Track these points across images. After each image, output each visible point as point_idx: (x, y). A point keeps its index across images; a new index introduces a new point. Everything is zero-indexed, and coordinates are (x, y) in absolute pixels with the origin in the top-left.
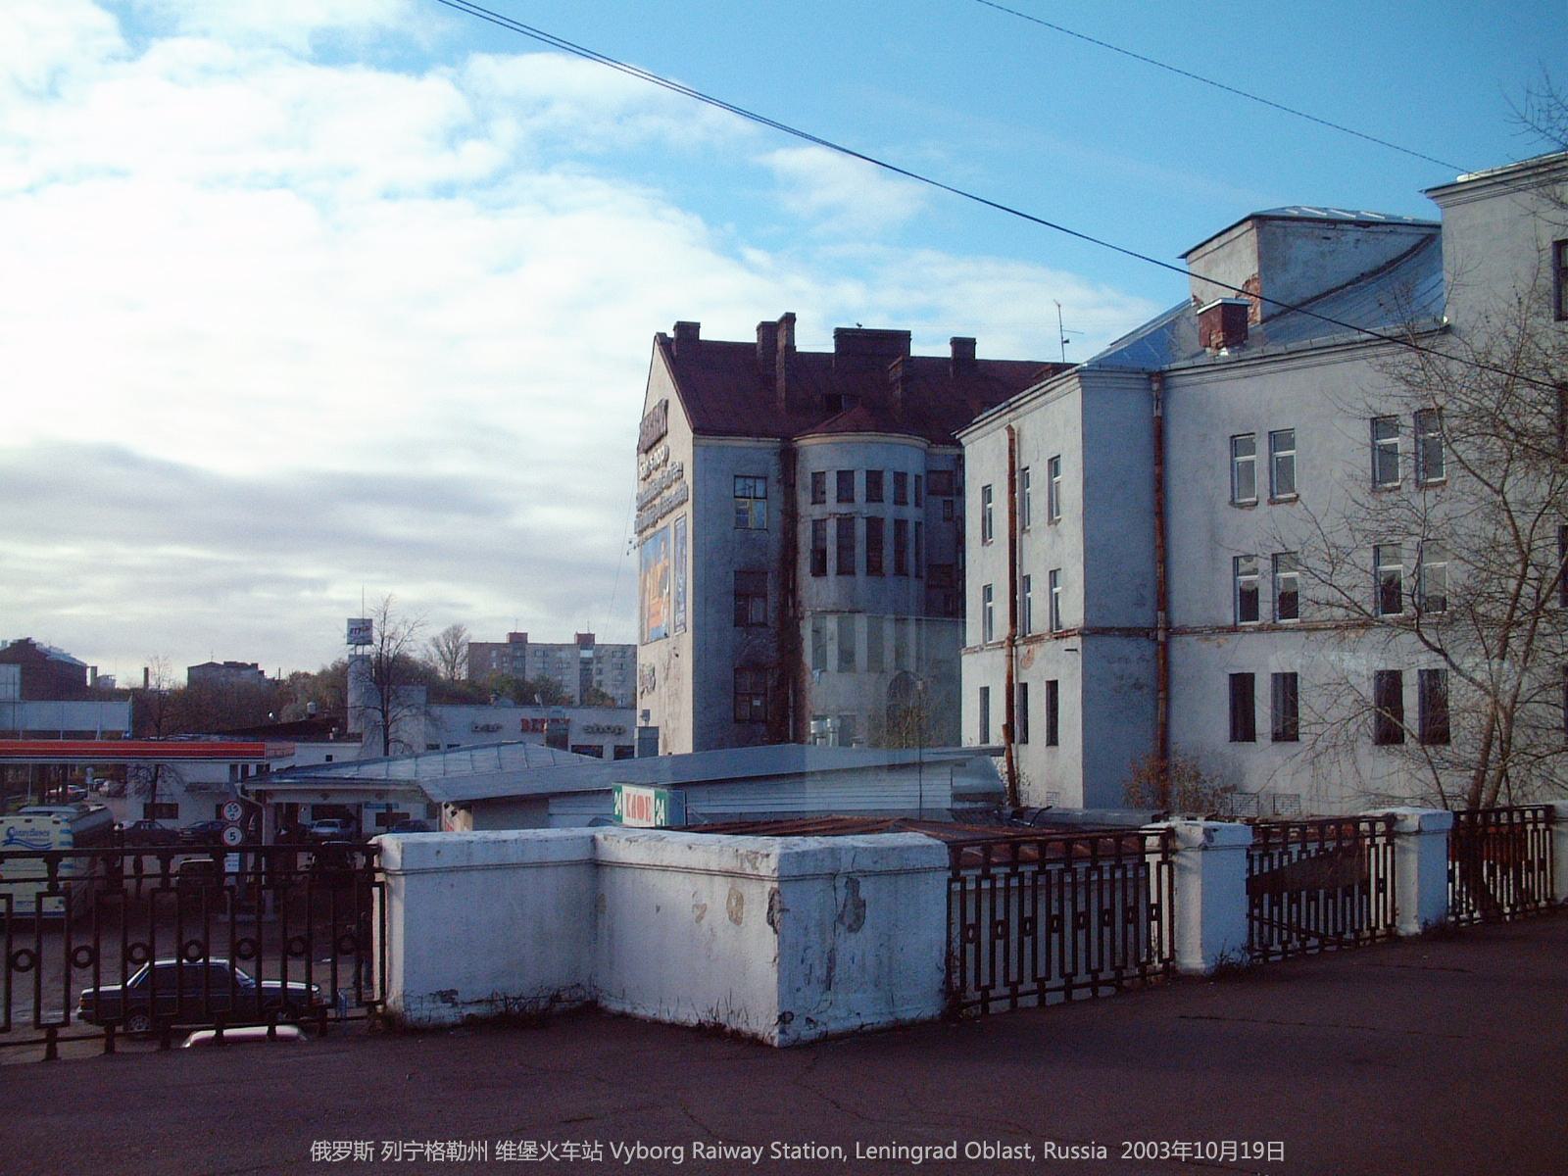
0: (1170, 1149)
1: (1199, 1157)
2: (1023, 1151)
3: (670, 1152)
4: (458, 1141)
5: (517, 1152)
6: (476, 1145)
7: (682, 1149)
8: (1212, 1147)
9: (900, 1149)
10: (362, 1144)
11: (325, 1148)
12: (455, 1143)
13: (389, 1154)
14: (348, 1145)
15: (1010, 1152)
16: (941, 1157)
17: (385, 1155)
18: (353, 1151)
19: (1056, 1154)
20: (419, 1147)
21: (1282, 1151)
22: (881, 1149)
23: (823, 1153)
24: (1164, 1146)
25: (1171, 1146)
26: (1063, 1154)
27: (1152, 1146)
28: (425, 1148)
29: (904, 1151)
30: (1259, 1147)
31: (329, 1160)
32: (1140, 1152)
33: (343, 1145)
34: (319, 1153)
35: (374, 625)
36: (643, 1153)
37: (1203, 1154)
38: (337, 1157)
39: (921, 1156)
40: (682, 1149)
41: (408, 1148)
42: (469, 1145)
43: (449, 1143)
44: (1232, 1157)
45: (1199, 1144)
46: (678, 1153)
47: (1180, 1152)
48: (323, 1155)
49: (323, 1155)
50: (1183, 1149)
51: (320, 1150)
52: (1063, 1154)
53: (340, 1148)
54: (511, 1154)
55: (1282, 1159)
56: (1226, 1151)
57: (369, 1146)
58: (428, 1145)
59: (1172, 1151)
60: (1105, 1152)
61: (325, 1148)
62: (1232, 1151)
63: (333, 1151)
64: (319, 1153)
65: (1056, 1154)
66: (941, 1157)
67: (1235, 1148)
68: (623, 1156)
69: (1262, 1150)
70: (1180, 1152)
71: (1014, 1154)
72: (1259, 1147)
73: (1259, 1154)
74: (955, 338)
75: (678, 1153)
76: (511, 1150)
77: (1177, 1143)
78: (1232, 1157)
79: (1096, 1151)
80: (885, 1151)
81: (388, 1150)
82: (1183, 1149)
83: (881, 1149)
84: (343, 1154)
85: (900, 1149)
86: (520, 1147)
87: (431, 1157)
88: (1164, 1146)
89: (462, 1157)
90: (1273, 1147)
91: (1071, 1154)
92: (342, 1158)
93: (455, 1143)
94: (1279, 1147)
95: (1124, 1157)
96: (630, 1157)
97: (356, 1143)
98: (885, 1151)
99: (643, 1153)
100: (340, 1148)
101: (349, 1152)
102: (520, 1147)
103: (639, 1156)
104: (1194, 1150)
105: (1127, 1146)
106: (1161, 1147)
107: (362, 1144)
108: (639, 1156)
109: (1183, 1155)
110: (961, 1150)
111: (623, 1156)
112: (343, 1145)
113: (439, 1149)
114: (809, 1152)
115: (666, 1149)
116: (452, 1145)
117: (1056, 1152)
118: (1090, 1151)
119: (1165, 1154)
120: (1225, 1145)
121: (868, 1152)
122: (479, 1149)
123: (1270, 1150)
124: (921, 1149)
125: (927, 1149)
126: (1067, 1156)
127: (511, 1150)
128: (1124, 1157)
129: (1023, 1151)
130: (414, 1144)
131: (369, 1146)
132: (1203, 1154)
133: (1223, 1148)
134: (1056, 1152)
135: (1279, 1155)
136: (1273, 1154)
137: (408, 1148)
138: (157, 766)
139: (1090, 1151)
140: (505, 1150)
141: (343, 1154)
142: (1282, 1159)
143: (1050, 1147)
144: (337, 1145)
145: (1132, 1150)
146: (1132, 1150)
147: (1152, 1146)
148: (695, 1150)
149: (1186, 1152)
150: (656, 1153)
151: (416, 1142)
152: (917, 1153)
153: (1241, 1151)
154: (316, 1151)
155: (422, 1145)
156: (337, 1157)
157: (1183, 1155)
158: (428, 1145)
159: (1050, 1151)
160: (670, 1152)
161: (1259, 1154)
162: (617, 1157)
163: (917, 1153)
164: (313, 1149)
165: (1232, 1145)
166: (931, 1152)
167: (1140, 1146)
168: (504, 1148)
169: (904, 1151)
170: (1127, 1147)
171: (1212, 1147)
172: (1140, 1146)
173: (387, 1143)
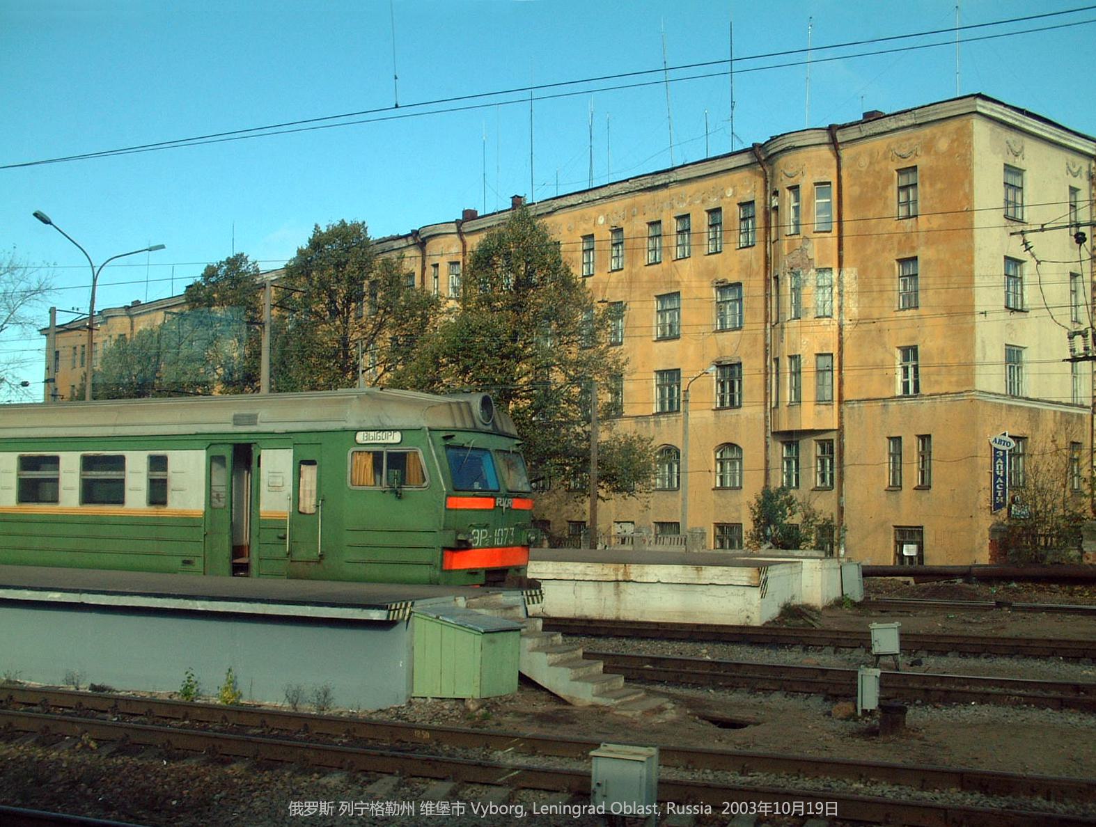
0: (756, 807)
1: (777, 813)
2: (652, 809)
3: (513, 808)
4: (393, 801)
5: (435, 809)
6: (406, 804)
7: (522, 807)
8: (786, 805)
9: (565, 807)
10: (325, 803)
11: (299, 806)
12: (391, 803)
13: (344, 811)
14: (315, 804)
15: (643, 809)
16: (594, 812)
17: (342, 811)
18: (319, 809)
19: (676, 811)
20: (366, 806)
21: (836, 808)
22: (551, 807)
23: (504, 810)
24: (753, 805)
25: (757, 804)
26: (681, 811)
27: (744, 805)
28: (370, 807)
29: (567, 809)
30: (819, 806)
31: (302, 815)
32: (735, 809)
33: (311, 804)
34: (295, 810)
35: (807, 284)
36: (494, 809)
37: (780, 810)
38: (307, 813)
39: (579, 812)
40: (522, 807)
41: (358, 806)
42: (401, 804)
43: (387, 803)
44: (801, 812)
45: (810, 803)
46: (519, 810)
47: (763, 809)
48: (297, 811)
49: (297, 811)
50: (766, 807)
51: (295, 808)
52: (681, 811)
53: (309, 806)
54: (431, 811)
55: (836, 814)
56: (796, 808)
57: (331, 805)
58: (372, 804)
59: (758, 809)
60: (710, 809)
61: (299, 806)
62: (801, 808)
63: (305, 809)
64: (295, 810)
65: (676, 811)
66: (594, 812)
67: (802, 806)
68: (481, 812)
69: (822, 808)
70: (763, 809)
71: (646, 811)
72: (819, 806)
73: (820, 811)
74: (167, 459)
75: (519, 810)
76: (431, 808)
77: (761, 803)
78: (801, 812)
79: (704, 808)
80: (554, 809)
81: (344, 808)
82: (766, 807)
83: (551, 807)
84: (312, 811)
85: (565, 807)
86: (437, 806)
87: (374, 812)
88: (753, 805)
89: (396, 812)
90: (829, 805)
91: (686, 810)
92: (311, 813)
93: (391, 803)
94: (834, 805)
95: (723, 813)
96: (485, 813)
97: (321, 803)
98: (554, 809)
99: (494, 809)
100: (309, 806)
101: (316, 810)
102: (437, 806)
103: (491, 812)
104: (774, 808)
105: (726, 805)
106: (750, 806)
107: (325, 803)
108: (491, 812)
109: (766, 811)
110: (608, 806)
111: (481, 812)
112: (311, 804)
113: (380, 807)
114: (576, 810)
115: (584, 807)
116: (389, 804)
117: (675, 809)
118: (699, 808)
119: (753, 811)
120: (796, 804)
121: (542, 809)
122: (408, 808)
123: (827, 808)
124: (579, 807)
125: (584, 807)
126: (683, 812)
127: (431, 808)
128: (723, 813)
129: (652, 809)
130: (362, 803)
131: (331, 805)
132: (780, 810)
133: (794, 806)
134: (675, 809)
135: (834, 811)
136: (830, 811)
137: (358, 806)
138: (375, 485)
139: (699, 808)
140: (427, 808)
141: (312, 811)
142: (836, 814)
143: (671, 805)
144: (307, 804)
145: (730, 808)
146: (730, 808)
147: (744, 805)
148: (669, 808)
149: (768, 809)
150: (504, 810)
151: (364, 802)
152: (576, 810)
153: (807, 808)
154: (293, 808)
155: (368, 804)
156: (307, 813)
157: (766, 811)
158: (372, 804)
159: (672, 808)
160: (513, 808)
161: (820, 811)
162: (476, 812)
163: (576, 810)
164: (290, 807)
165: (801, 804)
166: (587, 809)
167: (735, 805)
168: (426, 807)
169: (567, 809)
170: (726, 805)
171: (786, 805)
172: (735, 805)
173: (343, 803)
